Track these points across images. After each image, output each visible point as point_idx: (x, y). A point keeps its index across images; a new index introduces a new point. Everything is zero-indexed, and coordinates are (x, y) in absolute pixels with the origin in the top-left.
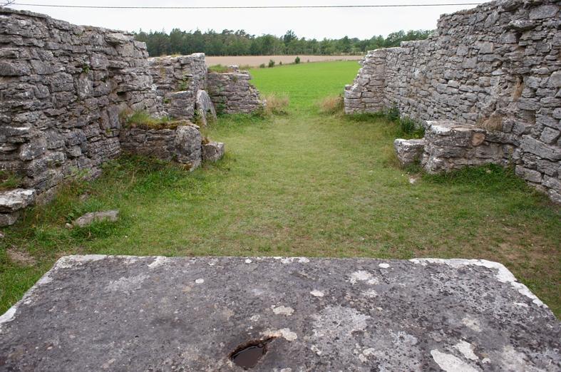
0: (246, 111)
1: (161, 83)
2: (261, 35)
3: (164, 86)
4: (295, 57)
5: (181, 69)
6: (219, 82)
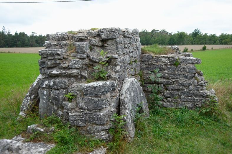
0: (190, 105)
1: (65, 68)
2: (176, 33)
3: (69, 72)
4: (203, 46)
5: (103, 47)
6: (156, 66)
